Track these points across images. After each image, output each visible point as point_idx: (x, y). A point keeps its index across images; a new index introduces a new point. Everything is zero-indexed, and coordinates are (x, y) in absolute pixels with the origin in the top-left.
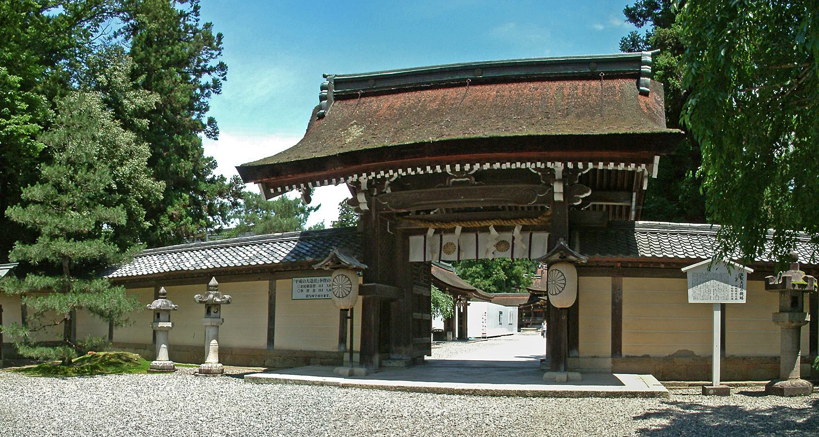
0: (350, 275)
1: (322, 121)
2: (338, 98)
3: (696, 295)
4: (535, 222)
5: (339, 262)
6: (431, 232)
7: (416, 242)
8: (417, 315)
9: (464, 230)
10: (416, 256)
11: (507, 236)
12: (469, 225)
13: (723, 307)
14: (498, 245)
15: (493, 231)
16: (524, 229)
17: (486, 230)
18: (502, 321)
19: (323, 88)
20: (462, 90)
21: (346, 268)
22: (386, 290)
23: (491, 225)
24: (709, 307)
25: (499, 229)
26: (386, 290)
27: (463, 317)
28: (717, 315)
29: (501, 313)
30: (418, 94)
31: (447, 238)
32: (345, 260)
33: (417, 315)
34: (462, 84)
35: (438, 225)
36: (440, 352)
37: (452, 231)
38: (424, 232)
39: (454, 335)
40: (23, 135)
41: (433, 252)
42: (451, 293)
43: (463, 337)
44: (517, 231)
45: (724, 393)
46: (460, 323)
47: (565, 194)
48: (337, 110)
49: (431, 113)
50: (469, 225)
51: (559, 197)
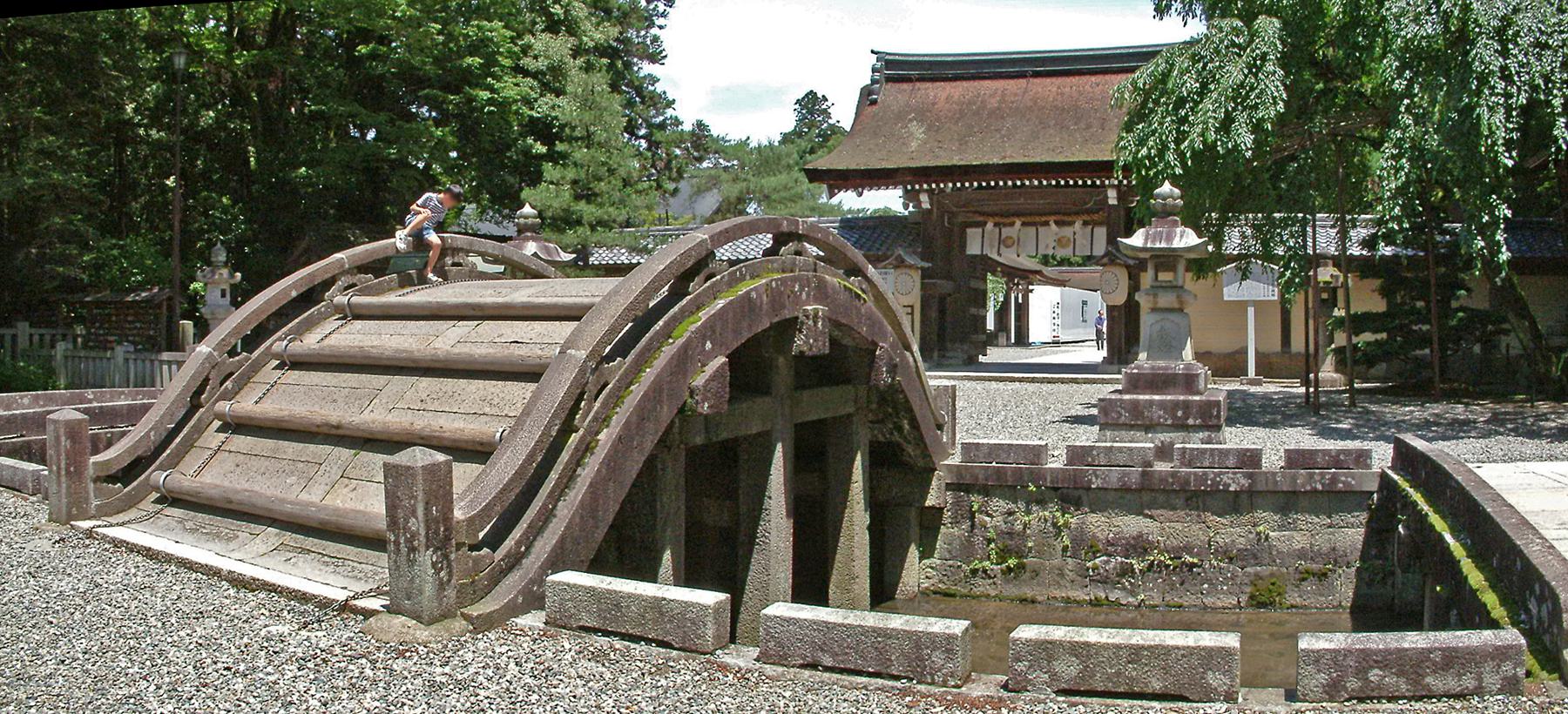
0: (912, 272)
1: (874, 108)
2: (889, 79)
3: (1231, 292)
4: (1095, 217)
5: (903, 261)
6: (990, 226)
7: (973, 234)
8: (973, 310)
9: (1024, 224)
10: (973, 249)
11: (1067, 232)
12: (1029, 219)
13: (1256, 304)
14: (1059, 241)
15: (1053, 226)
16: (1085, 223)
17: (1046, 224)
18: (1087, 317)
19: (874, 70)
20: (1023, 82)
21: (911, 267)
22: (945, 286)
23: (1052, 219)
24: (1242, 306)
25: (1057, 223)
26: (945, 286)
27: (1022, 310)
28: (1251, 310)
29: (1085, 303)
30: (976, 83)
31: (1006, 231)
32: (910, 260)
33: (973, 310)
34: (1022, 75)
35: (997, 219)
36: (994, 355)
37: (1012, 224)
38: (983, 224)
39: (1008, 338)
40: (516, 101)
41: (992, 246)
42: (1004, 274)
43: (1022, 340)
44: (1078, 225)
45: (1259, 383)
46: (1018, 319)
47: (1119, 199)
48: (894, 96)
49: (992, 113)
50: (1029, 219)
51: (1113, 201)
